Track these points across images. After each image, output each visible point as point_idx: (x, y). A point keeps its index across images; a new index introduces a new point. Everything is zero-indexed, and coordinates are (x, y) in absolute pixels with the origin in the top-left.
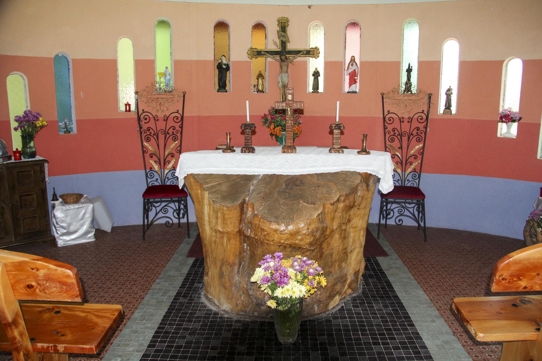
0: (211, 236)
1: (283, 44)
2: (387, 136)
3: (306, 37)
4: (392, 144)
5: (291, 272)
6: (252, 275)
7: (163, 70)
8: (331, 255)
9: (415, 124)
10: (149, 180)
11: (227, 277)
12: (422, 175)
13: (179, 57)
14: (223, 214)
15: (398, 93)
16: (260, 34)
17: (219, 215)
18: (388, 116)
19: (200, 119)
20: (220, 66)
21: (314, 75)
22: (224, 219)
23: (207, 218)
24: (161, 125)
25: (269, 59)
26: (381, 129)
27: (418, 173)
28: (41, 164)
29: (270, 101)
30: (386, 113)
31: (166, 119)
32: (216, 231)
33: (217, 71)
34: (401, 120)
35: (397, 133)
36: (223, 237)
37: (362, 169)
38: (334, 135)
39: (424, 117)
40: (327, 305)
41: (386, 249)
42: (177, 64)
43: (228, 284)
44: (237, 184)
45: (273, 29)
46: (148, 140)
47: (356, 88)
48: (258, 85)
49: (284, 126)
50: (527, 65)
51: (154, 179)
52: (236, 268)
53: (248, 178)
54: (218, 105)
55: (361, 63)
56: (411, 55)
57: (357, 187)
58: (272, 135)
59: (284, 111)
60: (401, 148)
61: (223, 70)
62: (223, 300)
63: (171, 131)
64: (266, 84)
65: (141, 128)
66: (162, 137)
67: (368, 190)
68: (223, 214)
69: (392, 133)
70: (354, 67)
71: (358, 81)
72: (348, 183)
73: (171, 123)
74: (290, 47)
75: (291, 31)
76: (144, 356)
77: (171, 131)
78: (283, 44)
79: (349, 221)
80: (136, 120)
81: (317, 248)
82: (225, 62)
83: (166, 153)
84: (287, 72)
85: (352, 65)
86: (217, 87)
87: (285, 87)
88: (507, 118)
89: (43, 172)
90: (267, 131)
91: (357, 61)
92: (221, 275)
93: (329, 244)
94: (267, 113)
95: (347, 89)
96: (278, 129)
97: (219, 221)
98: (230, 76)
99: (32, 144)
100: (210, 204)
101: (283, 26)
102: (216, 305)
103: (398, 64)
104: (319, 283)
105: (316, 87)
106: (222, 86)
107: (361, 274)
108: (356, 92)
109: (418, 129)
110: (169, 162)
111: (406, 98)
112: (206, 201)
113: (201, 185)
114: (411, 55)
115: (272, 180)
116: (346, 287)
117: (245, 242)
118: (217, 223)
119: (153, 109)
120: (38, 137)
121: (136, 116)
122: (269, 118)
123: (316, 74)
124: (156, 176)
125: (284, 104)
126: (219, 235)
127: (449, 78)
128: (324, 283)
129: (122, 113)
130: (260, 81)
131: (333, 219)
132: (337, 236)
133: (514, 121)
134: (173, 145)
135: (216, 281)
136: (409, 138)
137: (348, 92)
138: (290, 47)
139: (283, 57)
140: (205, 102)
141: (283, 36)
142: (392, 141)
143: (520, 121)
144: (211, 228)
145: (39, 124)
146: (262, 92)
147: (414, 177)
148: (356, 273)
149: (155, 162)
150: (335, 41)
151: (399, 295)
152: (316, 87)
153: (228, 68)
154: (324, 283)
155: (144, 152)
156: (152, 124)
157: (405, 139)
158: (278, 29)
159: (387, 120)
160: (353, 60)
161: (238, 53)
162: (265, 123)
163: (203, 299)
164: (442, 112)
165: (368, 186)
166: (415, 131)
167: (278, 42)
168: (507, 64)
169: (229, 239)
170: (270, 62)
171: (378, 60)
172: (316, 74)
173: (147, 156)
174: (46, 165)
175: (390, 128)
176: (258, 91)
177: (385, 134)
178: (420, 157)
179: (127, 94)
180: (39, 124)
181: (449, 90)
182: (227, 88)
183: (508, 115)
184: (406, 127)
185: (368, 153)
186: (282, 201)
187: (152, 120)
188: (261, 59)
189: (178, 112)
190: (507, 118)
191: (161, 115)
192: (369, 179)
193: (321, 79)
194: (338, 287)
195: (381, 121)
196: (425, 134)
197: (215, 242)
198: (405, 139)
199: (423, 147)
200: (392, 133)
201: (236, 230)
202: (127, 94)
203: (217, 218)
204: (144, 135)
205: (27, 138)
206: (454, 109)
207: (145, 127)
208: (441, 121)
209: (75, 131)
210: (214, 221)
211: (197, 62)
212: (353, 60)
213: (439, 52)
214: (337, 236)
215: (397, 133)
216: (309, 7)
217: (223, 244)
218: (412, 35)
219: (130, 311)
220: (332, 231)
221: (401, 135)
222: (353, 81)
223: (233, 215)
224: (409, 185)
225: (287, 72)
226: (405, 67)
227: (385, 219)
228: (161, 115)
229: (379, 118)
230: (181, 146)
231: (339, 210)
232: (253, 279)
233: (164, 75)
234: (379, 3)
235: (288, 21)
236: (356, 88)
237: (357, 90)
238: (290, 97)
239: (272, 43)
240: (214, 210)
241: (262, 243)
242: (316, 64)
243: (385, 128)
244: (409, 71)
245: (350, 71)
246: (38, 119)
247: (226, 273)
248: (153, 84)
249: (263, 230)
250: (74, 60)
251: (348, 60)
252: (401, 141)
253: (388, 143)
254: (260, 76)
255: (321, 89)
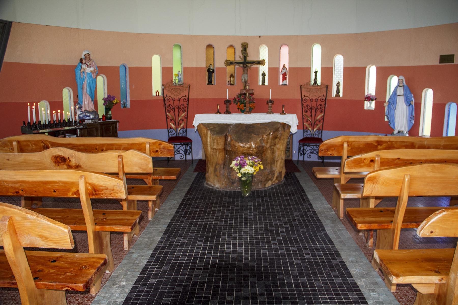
0: (211, 152)
1: (245, 58)
2: (304, 109)
3: (257, 53)
4: (306, 114)
5: (248, 162)
6: (231, 164)
7: (177, 73)
8: (267, 160)
9: (319, 103)
10: (170, 134)
11: (218, 171)
12: (323, 131)
13: (186, 66)
14: (217, 140)
15: (310, 85)
16: (232, 50)
17: (215, 141)
18: (304, 98)
19: (197, 100)
20: (209, 70)
21: (262, 75)
22: (217, 143)
23: (209, 143)
24: (176, 103)
25: (237, 66)
26: (300, 106)
27: (321, 130)
28: (115, 123)
29: (238, 89)
30: (303, 96)
31: (179, 100)
32: (213, 149)
33: (207, 73)
34: (311, 100)
35: (309, 108)
36: (216, 152)
37: (281, 121)
38: (269, 106)
39: (324, 98)
40: (265, 185)
41: (300, 170)
42: (186, 70)
43: (219, 174)
44: (221, 129)
45: (239, 49)
46: (169, 112)
47: (287, 82)
48: (230, 81)
49: (245, 101)
50: (378, 69)
51: (173, 133)
52: (222, 166)
53: (228, 125)
54: (209, 93)
55: (289, 68)
56: (317, 64)
57: (278, 128)
58: (238, 108)
59: (245, 94)
60: (311, 116)
61: (210, 72)
62: (216, 182)
63: (182, 107)
64: (235, 80)
65: (165, 105)
66: (177, 110)
67: (284, 131)
68: (217, 140)
69: (306, 108)
70: (285, 71)
71: (287, 78)
72: (274, 127)
73: (182, 102)
74: (249, 59)
75: (249, 50)
76: (127, 299)
77: (182, 107)
78: (245, 58)
79: (275, 145)
80: (163, 101)
81: (260, 153)
82: (212, 67)
83: (179, 119)
84: (247, 74)
85: (284, 69)
86: (207, 82)
87: (246, 82)
88: (369, 98)
89: (116, 127)
90: (236, 107)
91: (287, 67)
92: (215, 170)
93: (265, 154)
94: (236, 97)
95: (281, 83)
96: (242, 105)
97: (215, 144)
98: (214, 76)
99: (110, 112)
100: (210, 137)
101: (245, 47)
102: (212, 186)
103: (308, 70)
104: (260, 168)
105: (263, 82)
106: (210, 82)
107: (283, 175)
108: (286, 85)
109: (321, 105)
110: (181, 124)
111: (314, 88)
112: (209, 135)
113: (206, 128)
114: (317, 64)
115: (239, 126)
116: (275, 179)
117: (227, 154)
118: (214, 145)
119: (172, 95)
120: (114, 108)
121: (163, 98)
122: (237, 99)
123: (264, 75)
124: (174, 132)
125: (245, 91)
126: (215, 151)
127: (338, 76)
128: (262, 168)
129: (154, 96)
130: (232, 78)
131: (267, 142)
132: (269, 151)
133: (373, 100)
134: (183, 115)
135: (213, 175)
136: (316, 110)
137: (282, 85)
138: (249, 59)
139: (245, 65)
140: (201, 90)
141: (245, 53)
142: (306, 112)
143: (376, 100)
144: (211, 148)
145: (115, 102)
146: (233, 85)
147: (318, 132)
148: (280, 173)
149: (173, 124)
150: (275, 54)
151: (302, 184)
152: (263, 82)
153: (213, 72)
154: (262, 168)
155: (167, 118)
156: (171, 103)
157: (314, 111)
158: (242, 49)
159: (303, 100)
160: (284, 66)
161: (219, 63)
162: (235, 102)
163: (205, 185)
164: (334, 96)
165: (284, 129)
166: (319, 106)
167: (242, 56)
168: (369, 70)
169: (219, 153)
170: (237, 68)
171: (299, 67)
172: (264, 75)
173: (169, 120)
174: (118, 123)
175: (305, 105)
176: (231, 84)
177: (302, 108)
178: (322, 121)
179: (157, 87)
180: (115, 102)
181: (338, 83)
182: (213, 83)
183: (369, 97)
184: (314, 104)
185: (285, 114)
186: (244, 134)
187: (172, 101)
188: (232, 67)
189: (186, 96)
190: (369, 98)
191: (176, 98)
192: (285, 126)
193: (266, 78)
194: (270, 176)
195: (300, 101)
196: (325, 108)
197: (213, 154)
198: (314, 111)
199: (324, 116)
200: (306, 108)
201: (223, 148)
202: (157, 87)
203: (214, 142)
204: (167, 109)
205: (108, 109)
206: (341, 94)
207: (167, 104)
208: (334, 100)
209: (129, 106)
210: (213, 144)
211: (196, 68)
212: (284, 66)
213: (332, 61)
214: (269, 151)
215: (309, 108)
216: (260, 37)
217: (216, 155)
218: (317, 51)
219: (87, 301)
220: (267, 148)
221: (311, 109)
222: (284, 79)
223: (221, 141)
224: (316, 137)
225: (247, 74)
226: (314, 71)
227: (302, 156)
228: (176, 98)
229: (299, 99)
230: (187, 115)
231: (270, 139)
232: (231, 166)
233: (178, 75)
234: (298, 34)
235: (247, 44)
236: (287, 82)
237: (287, 84)
238: (247, 87)
239: (239, 57)
240: (213, 139)
241: (235, 153)
242: (264, 69)
243: (302, 105)
244: (316, 72)
245: (283, 72)
246: (114, 99)
247: (218, 169)
248: (172, 81)
249: (235, 146)
250: (130, 68)
251: (282, 67)
252: (311, 112)
253: (304, 113)
254: (232, 76)
255: (266, 83)
